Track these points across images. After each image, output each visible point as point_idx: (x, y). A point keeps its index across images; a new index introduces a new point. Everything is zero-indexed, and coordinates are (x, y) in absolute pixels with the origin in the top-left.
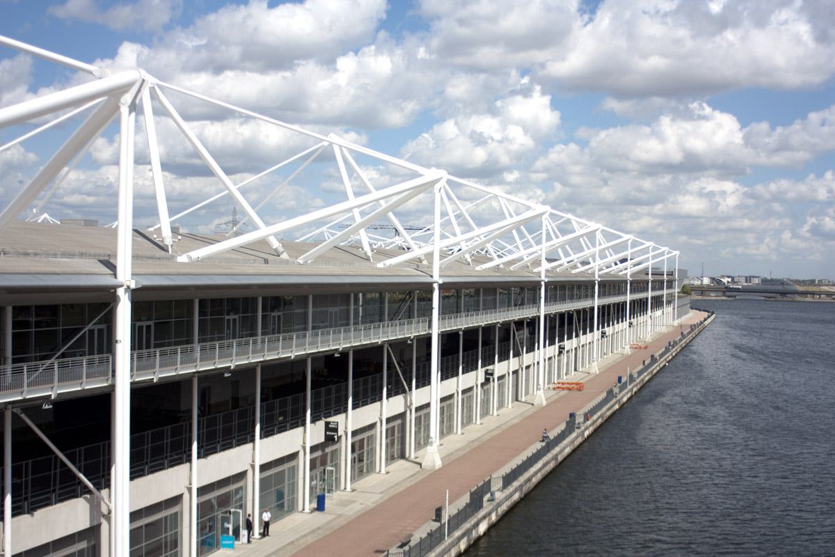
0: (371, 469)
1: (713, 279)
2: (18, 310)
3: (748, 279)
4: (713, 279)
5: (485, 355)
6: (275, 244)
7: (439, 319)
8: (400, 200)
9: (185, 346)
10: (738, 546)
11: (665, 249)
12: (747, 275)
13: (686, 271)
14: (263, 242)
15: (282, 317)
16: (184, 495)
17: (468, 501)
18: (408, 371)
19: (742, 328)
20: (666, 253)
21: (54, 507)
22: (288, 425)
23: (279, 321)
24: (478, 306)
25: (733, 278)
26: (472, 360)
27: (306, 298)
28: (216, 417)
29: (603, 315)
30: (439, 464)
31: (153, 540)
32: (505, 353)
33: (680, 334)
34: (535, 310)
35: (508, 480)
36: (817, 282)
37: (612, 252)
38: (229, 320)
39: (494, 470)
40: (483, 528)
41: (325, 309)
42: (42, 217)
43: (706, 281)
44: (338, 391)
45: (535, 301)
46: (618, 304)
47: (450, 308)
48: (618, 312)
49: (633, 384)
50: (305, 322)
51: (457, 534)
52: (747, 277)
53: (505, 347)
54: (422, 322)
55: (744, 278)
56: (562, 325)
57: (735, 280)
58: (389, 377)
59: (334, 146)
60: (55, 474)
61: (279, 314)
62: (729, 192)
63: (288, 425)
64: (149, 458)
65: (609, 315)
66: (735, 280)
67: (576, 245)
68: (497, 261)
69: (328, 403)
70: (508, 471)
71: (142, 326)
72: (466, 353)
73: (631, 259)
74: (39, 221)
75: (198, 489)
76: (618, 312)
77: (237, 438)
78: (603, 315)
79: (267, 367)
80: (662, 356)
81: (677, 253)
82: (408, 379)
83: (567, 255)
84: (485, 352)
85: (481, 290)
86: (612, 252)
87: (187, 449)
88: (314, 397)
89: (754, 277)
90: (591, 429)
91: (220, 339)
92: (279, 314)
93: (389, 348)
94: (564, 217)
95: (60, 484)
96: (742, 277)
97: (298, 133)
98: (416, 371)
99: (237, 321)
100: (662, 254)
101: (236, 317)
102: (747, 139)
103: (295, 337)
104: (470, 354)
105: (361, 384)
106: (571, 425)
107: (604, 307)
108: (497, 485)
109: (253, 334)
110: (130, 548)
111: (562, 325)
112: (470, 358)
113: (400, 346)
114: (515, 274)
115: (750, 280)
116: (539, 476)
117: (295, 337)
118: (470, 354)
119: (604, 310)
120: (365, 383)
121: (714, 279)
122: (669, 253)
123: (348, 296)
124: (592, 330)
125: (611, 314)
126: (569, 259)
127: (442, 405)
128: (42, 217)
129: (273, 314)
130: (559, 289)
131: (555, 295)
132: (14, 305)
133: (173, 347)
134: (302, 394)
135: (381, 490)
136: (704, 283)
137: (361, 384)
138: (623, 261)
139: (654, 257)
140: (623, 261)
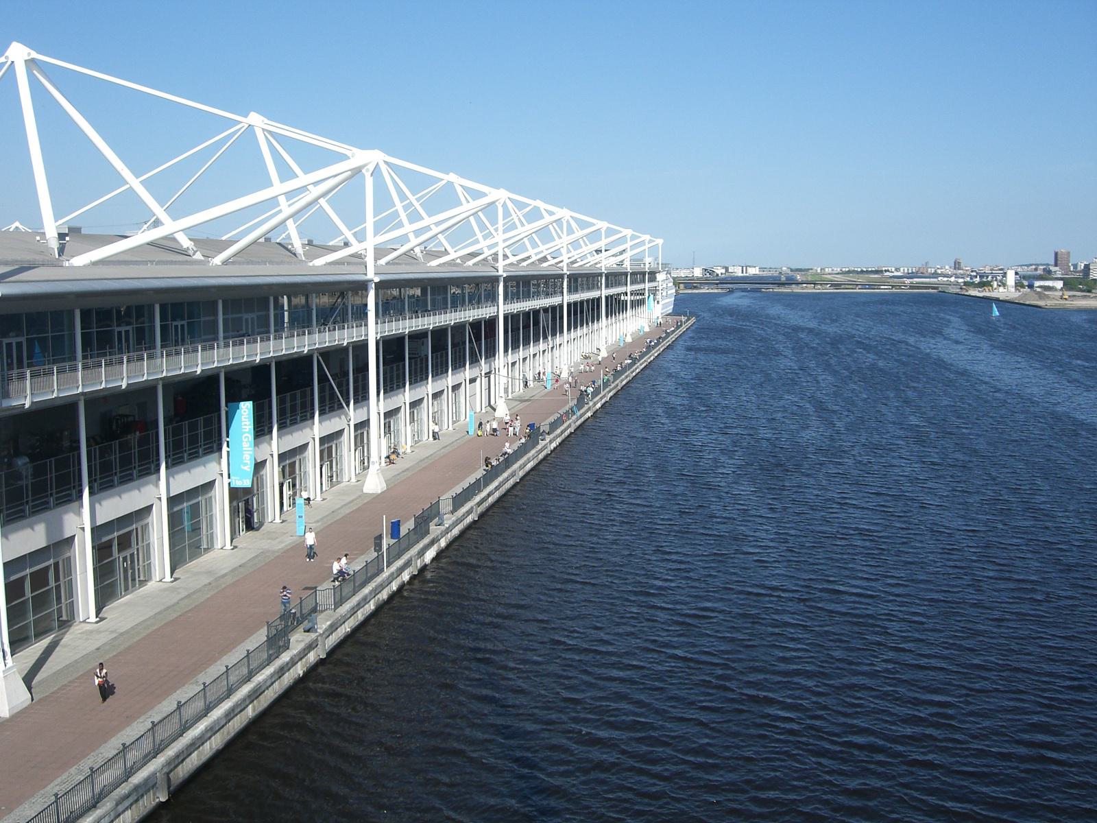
0: (136, 576)
2: (86, 315)
5: (437, 363)
6: (185, 243)
7: (377, 323)
9: (61, 365)
11: (647, 237)
13: (26, 61)
14: (170, 238)
15: (186, 327)
16: (217, 482)
17: (412, 527)
18: (344, 384)
20: (647, 242)
21: (53, 511)
22: (186, 455)
23: (253, 323)
24: (447, 304)
26: (398, 376)
27: (214, 304)
28: (69, 457)
29: (575, 314)
30: (631, 341)
31: (16, 602)
32: (442, 365)
33: (482, 462)
34: (560, 298)
35: (459, 501)
37: (587, 242)
38: (120, 333)
39: (444, 492)
40: (430, 555)
41: (239, 315)
42: (13, 226)
43: (698, 273)
44: (304, 396)
45: (492, 298)
46: (593, 300)
47: (388, 308)
48: (593, 310)
49: (608, 390)
50: (216, 332)
51: (399, 563)
53: (460, 352)
54: (357, 326)
56: (526, 327)
58: (321, 391)
59: (256, 128)
60: (51, 478)
61: (183, 322)
63: (186, 455)
64: (118, 467)
65: (582, 312)
67: (544, 234)
68: (453, 255)
69: (194, 441)
70: (459, 490)
71: (11, 343)
72: (434, 355)
73: (606, 251)
74: (11, 230)
75: (320, 439)
76: (593, 310)
77: (55, 496)
78: (575, 314)
79: (95, 401)
80: (554, 426)
81: (660, 241)
82: (345, 391)
83: (535, 245)
84: (455, 353)
85: (429, 288)
86: (587, 242)
87: (77, 483)
88: (281, 402)
90: (559, 440)
91: (104, 355)
92: (19, 339)
93: (320, 358)
94: (529, 205)
95: (139, 462)
98: (354, 383)
99: (131, 332)
100: (643, 243)
101: (129, 328)
103: (200, 349)
104: (395, 368)
105: (288, 399)
106: (534, 434)
107: (575, 303)
108: (445, 506)
109: (216, 339)
110: (7, 604)
111: (526, 327)
112: (439, 360)
113: (333, 355)
114: (471, 268)
116: (497, 495)
117: (200, 349)
118: (395, 368)
119: (575, 308)
120: (293, 398)
121: (706, 270)
122: (650, 241)
123: (266, 300)
124: (562, 332)
125: (584, 314)
126: (570, 255)
127: (322, 448)
128: (13, 226)
129: (175, 323)
130: (521, 285)
131: (518, 292)
133: (97, 359)
134: (216, 414)
135: (316, 519)
137: (288, 399)
138: (598, 251)
139: (633, 247)
140: (598, 251)
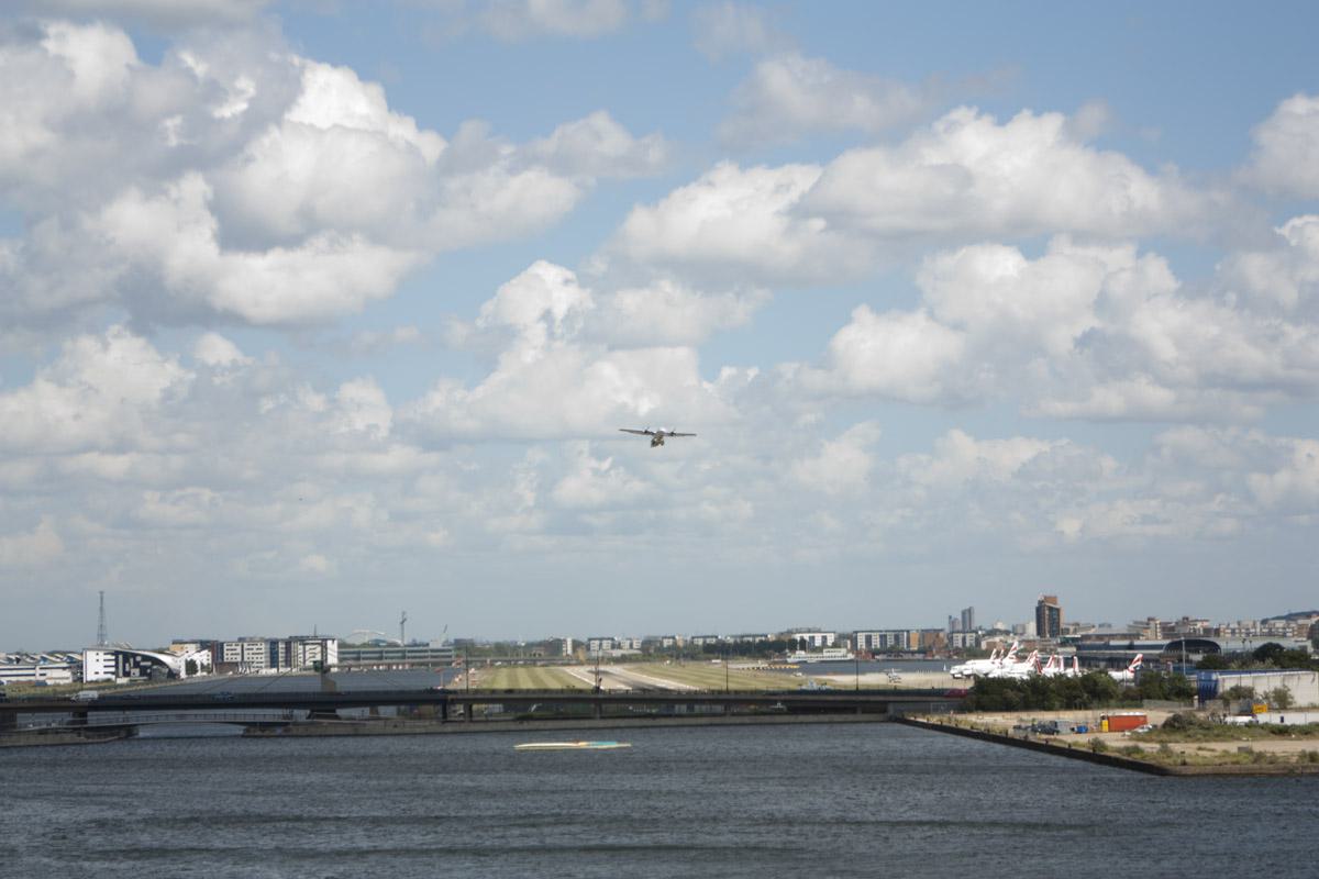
1: (124, 658)
3: (279, 650)
4: (124, 658)
8: (836, 673)
10: (764, 709)
12: (283, 633)
13: (1253, 689)
19: (513, 720)
25: (215, 648)
36: (569, 649)
43: (97, 667)
52: (274, 643)
55: (264, 647)
57: (228, 657)
62: (22, 849)
66: (228, 657)
89: (303, 641)
96: (252, 641)
97: (361, 732)
102: (1107, 674)
115: (288, 650)
121: (127, 656)
132: (576, 638)
136: (90, 676)
